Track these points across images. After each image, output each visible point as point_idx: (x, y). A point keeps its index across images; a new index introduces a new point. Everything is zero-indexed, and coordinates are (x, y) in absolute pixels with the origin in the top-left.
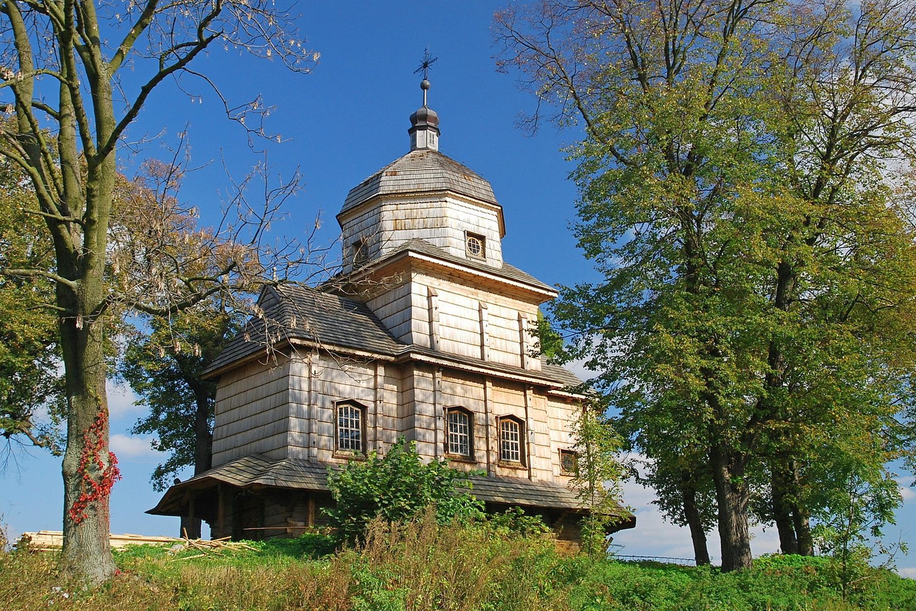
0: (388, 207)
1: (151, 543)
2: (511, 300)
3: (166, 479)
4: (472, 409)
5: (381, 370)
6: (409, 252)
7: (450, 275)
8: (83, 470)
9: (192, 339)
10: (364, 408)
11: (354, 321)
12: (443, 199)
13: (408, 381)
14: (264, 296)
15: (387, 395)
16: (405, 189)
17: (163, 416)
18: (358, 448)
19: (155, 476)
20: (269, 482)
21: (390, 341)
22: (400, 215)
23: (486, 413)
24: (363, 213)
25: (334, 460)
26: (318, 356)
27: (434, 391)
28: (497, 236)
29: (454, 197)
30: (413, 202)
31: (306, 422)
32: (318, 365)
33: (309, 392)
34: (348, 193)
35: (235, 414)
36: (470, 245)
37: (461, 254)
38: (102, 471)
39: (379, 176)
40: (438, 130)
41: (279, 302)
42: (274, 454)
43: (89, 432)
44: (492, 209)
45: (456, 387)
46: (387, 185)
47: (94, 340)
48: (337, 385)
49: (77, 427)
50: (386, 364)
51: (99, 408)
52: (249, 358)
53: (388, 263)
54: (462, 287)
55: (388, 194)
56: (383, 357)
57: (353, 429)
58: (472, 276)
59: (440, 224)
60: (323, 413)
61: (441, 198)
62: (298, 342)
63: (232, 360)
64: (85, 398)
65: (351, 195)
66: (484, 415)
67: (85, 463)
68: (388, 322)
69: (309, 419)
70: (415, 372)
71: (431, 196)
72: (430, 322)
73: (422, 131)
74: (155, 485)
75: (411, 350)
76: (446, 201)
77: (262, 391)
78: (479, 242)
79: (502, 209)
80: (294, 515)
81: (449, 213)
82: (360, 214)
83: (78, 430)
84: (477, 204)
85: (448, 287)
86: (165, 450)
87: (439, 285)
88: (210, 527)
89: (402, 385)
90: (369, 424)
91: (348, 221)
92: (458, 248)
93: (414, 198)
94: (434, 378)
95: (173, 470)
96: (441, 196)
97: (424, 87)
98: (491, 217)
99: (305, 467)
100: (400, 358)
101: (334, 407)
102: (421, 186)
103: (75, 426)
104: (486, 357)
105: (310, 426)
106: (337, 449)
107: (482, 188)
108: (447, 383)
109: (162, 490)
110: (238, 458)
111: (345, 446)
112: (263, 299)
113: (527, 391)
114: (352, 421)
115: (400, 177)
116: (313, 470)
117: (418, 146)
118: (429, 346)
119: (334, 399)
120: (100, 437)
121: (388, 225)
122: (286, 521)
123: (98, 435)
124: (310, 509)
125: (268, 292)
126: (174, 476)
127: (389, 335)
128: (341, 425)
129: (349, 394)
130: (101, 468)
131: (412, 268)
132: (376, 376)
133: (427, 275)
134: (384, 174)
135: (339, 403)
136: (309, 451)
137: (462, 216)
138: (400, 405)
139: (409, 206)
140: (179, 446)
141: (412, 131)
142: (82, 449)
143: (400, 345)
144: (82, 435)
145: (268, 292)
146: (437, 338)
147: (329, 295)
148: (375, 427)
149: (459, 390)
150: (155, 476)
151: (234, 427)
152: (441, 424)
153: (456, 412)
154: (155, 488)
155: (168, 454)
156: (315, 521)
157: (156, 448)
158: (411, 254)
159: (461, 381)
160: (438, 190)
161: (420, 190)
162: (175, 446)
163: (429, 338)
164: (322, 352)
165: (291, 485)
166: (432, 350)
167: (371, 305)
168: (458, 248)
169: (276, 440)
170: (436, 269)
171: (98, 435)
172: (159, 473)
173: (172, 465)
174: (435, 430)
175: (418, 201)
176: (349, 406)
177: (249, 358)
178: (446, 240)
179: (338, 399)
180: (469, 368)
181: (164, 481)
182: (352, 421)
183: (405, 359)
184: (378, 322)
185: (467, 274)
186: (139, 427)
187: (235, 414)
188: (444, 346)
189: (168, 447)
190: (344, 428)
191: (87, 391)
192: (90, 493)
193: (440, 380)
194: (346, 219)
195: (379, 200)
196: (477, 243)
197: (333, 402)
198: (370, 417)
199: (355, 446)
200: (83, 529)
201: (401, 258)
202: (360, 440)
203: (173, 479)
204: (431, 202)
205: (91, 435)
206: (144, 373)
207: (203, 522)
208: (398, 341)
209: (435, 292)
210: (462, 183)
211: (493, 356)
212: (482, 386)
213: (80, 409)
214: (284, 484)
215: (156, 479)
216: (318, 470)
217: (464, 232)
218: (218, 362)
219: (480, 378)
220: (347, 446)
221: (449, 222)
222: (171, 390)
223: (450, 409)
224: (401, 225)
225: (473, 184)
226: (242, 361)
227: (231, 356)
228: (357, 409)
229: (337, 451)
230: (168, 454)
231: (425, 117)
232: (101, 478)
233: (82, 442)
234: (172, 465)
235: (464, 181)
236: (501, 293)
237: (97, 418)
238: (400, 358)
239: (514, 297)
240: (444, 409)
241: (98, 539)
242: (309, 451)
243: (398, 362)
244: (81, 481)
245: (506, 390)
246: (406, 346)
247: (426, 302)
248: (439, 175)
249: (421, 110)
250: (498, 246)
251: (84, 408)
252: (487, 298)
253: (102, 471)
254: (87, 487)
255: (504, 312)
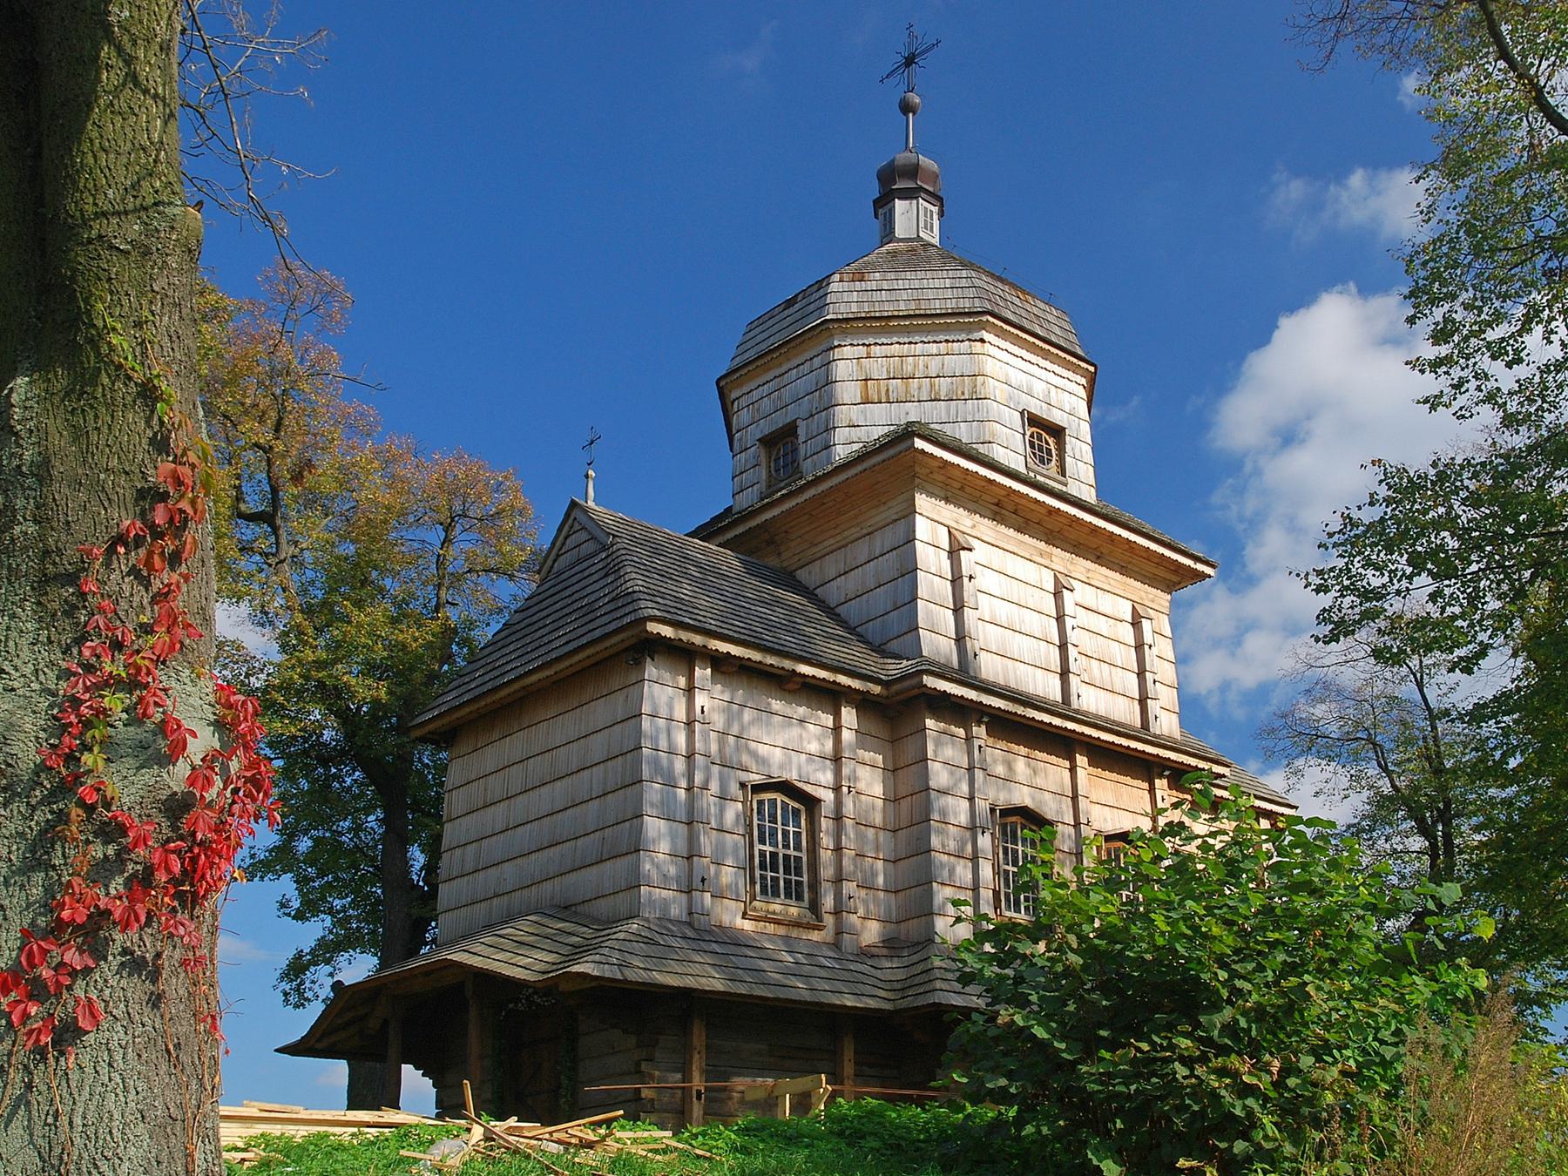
0: (847, 351)
1: (338, 1130)
2: (1117, 576)
3: (313, 982)
4: (1050, 816)
5: (849, 715)
6: (916, 440)
7: (997, 505)
8: (71, 758)
9: (371, 669)
10: (812, 803)
11: (779, 602)
12: (976, 335)
13: (910, 747)
14: (566, 538)
15: (864, 773)
16: (889, 309)
17: (304, 844)
18: (799, 898)
19: (287, 975)
20: (608, 971)
21: (864, 651)
22: (877, 368)
23: (1077, 825)
24: (785, 368)
25: (748, 925)
26: (709, 670)
27: (970, 769)
28: (1085, 430)
29: (1001, 334)
30: (907, 340)
31: (683, 829)
32: (711, 697)
33: (690, 757)
34: (744, 330)
35: (496, 816)
36: (1032, 445)
37: (1017, 462)
38: (182, 769)
39: (822, 283)
40: (940, 199)
41: (604, 548)
42: (603, 907)
43: (107, 564)
44: (1075, 369)
45: (1015, 760)
46: (845, 298)
47: (133, 78)
48: (753, 745)
49: (42, 537)
50: (863, 703)
51: (161, 445)
52: (534, 678)
53: (859, 468)
54: (1020, 536)
55: (847, 320)
56: (855, 684)
57: (788, 852)
58: (1043, 511)
59: (970, 390)
60: (722, 811)
61: (970, 331)
62: (667, 631)
63: (489, 686)
64: (83, 382)
65: (752, 334)
66: (1072, 830)
67: (88, 725)
68: (851, 611)
69: (689, 824)
70: (930, 723)
71: (947, 328)
72: (958, 610)
73: (908, 202)
74: (286, 994)
75: (923, 667)
76: (982, 341)
77: (569, 757)
78: (1051, 441)
79: (1095, 373)
80: (657, 1055)
81: (990, 366)
82: (777, 372)
83: (46, 553)
84: (1046, 355)
85: (990, 533)
86: (308, 919)
87: (974, 527)
88: (434, 1086)
89: (894, 756)
90: (826, 841)
91: (746, 389)
92: (1011, 449)
93: (908, 331)
94: (969, 739)
95: (328, 962)
96: (970, 328)
97: (906, 108)
98: (1072, 387)
99: (684, 938)
100: (896, 688)
101: (745, 797)
102: (923, 305)
103: (32, 528)
104: (1074, 698)
105: (692, 840)
106: (754, 898)
107: (1056, 324)
108: (996, 753)
109: (303, 1005)
110: (509, 918)
111: (770, 890)
112: (563, 544)
113: (1157, 781)
114: (785, 834)
115: (874, 285)
116: (704, 946)
117: (899, 233)
118: (955, 664)
119: (744, 776)
120: (161, 597)
121: (847, 391)
122: (639, 1072)
123: (157, 585)
124: (696, 1042)
125: (577, 527)
126: (331, 975)
127: (860, 639)
128: (762, 841)
129: (781, 767)
130: (179, 748)
131: (917, 481)
132: (837, 729)
133: (947, 500)
134: (837, 277)
135: (757, 789)
136: (690, 901)
137: (1017, 378)
138: (892, 799)
139: (896, 349)
140: (338, 912)
141: (883, 203)
142: (66, 651)
143: (890, 661)
144: (72, 579)
145: (577, 527)
146: (973, 645)
147: (714, 548)
148: (838, 849)
149: (1020, 765)
150: (287, 975)
151: (495, 847)
152: (985, 841)
153: (1013, 819)
154: (286, 1001)
155: (315, 930)
156: (707, 1071)
157: (288, 915)
158: (919, 443)
159: (1023, 750)
160: (965, 314)
161: (922, 312)
162: (331, 912)
163: (954, 648)
164: (720, 664)
165: (660, 978)
166: (964, 673)
167: (802, 575)
168: (1011, 449)
169: (612, 871)
170: (968, 489)
171: (157, 585)
172: (297, 968)
173: (327, 951)
174: (975, 859)
175: (917, 339)
176: (780, 798)
177: (534, 678)
178: (984, 427)
179: (756, 778)
180: (1046, 718)
181: (307, 984)
182: (785, 834)
183: (909, 689)
184: (831, 612)
185: (1034, 507)
186: (251, 865)
187: (496, 816)
188: (990, 668)
189: (315, 912)
190: (768, 848)
191: (93, 343)
192: (117, 885)
193: (982, 743)
194: (741, 385)
195: (826, 333)
196: (1047, 443)
197: (743, 785)
198: (825, 824)
199: (794, 892)
200: (74, 1076)
201: (896, 455)
202: (805, 878)
203: (330, 981)
204: (947, 341)
205: (118, 579)
206: (263, 746)
207: (407, 1069)
208: (881, 650)
209: (967, 541)
210: (1013, 304)
211: (1089, 700)
212: (1067, 764)
213: (59, 440)
214: (642, 976)
215: (291, 981)
216: (715, 947)
217: (1022, 413)
218: (454, 694)
219: (1062, 744)
220: (776, 894)
221: (993, 388)
222: (322, 791)
223: (1006, 812)
224: (879, 392)
225: (1035, 310)
226: (516, 686)
227: (487, 678)
228: (796, 805)
229: (755, 903)
230: (315, 930)
231: (913, 171)
232: (176, 807)
233: (71, 610)
234: (327, 951)
235: (1017, 301)
236: (1099, 559)
237: (150, 496)
238: (896, 688)
239: (1124, 570)
240: (992, 810)
241: (161, 1130)
242: (690, 901)
243: (887, 697)
244: (62, 817)
245: (1114, 776)
246: (905, 663)
247: (946, 564)
248: (964, 283)
249: (903, 158)
250: (1086, 452)
251: (78, 434)
252: (1071, 568)
253: (182, 769)
254: (97, 851)
255: (1107, 603)
